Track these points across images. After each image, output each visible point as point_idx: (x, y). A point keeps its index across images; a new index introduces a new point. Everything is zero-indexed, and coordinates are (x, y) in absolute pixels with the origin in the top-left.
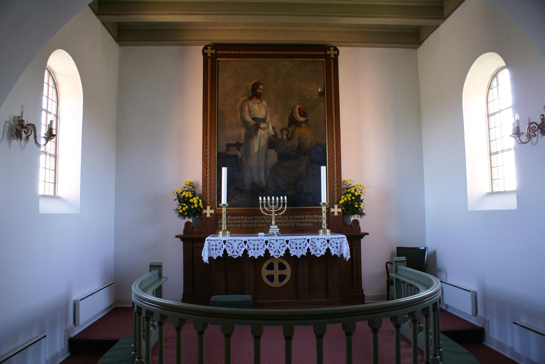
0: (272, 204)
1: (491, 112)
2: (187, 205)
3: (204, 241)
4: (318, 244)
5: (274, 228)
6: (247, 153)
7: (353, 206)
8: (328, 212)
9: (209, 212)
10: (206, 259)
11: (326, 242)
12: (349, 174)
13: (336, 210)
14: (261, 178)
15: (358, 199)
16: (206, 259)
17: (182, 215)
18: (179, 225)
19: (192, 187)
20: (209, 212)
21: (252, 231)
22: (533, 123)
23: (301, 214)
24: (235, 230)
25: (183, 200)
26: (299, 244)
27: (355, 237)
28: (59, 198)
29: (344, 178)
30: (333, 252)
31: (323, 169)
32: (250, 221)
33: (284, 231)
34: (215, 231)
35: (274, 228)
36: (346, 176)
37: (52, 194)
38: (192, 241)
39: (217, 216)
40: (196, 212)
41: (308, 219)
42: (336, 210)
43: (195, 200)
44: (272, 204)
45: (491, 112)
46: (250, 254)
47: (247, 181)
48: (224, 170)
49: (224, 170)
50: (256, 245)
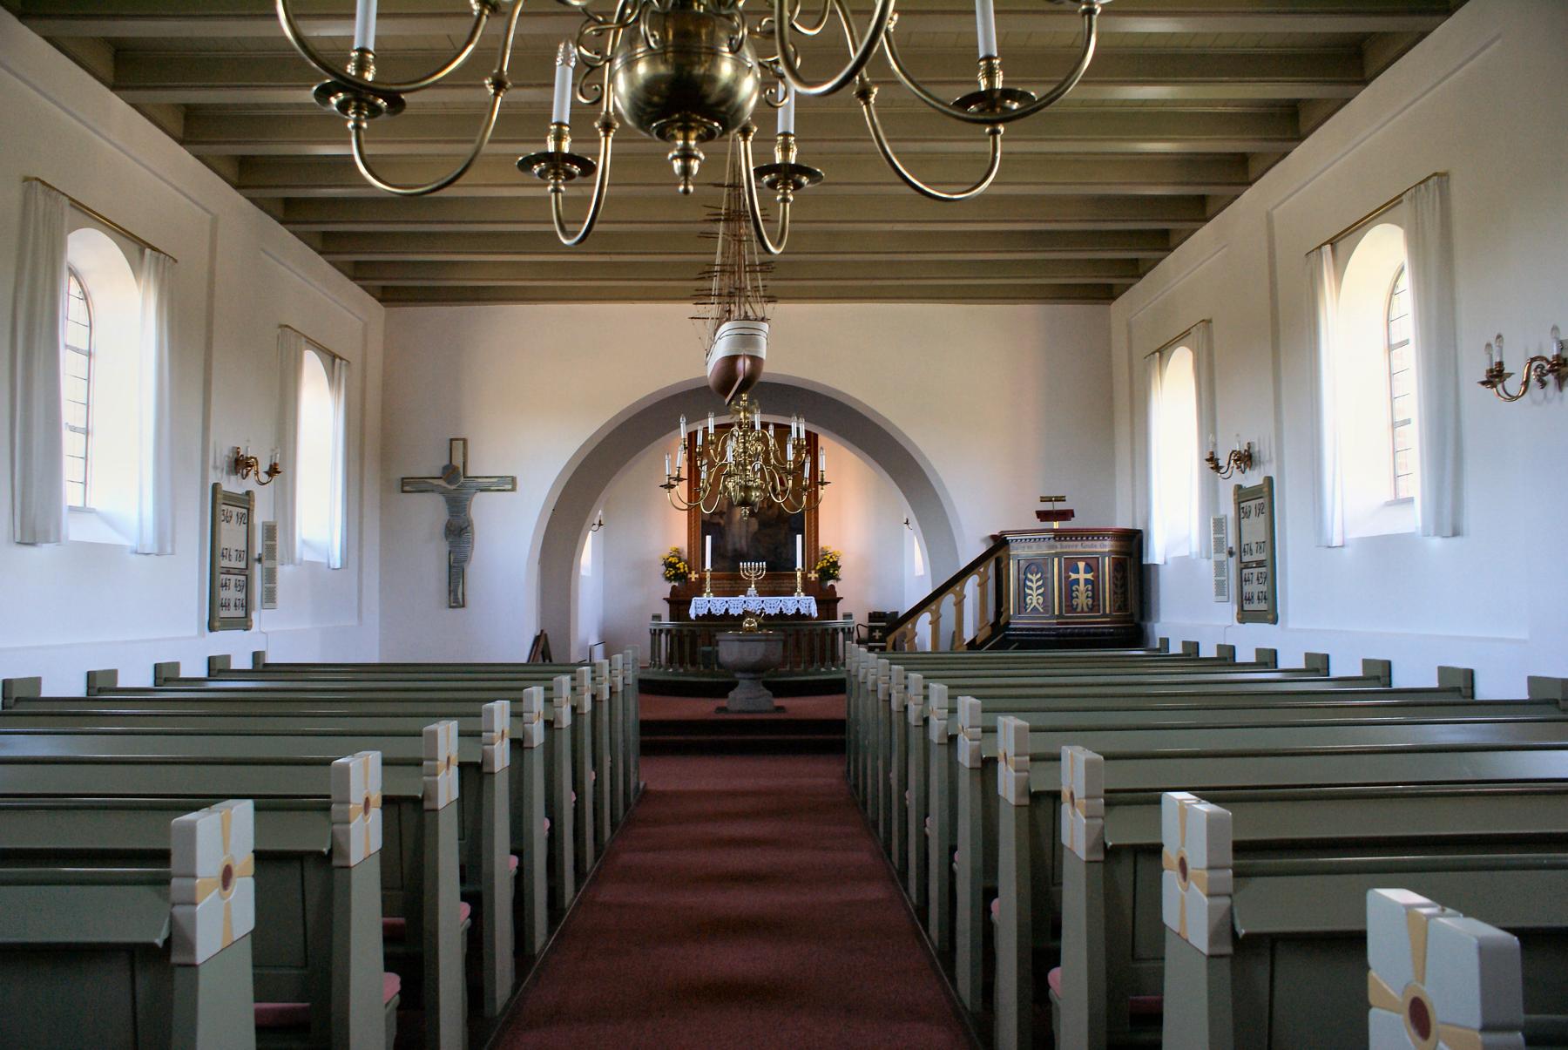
0: (752, 569)
1: (1394, 341)
2: (675, 572)
3: (689, 603)
4: (790, 604)
5: (752, 589)
6: (730, 521)
7: (830, 570)
8: (804, 577)
9: (694, 576)
10: (693, 616)
11: (804, 603)
12: (827, 540)
13: (813, 576)
14: (742, 544)
15: (835, 565)
16: (693, 616)
17: (669, 579)
18: (666, 588)
19: (677, 553)
20: (694, 576)
21: (734, 593)
22: (1533, 360)
23: (778, 579)
24: (718, 593)
25: (669, 565)
26: (773, 605)
27: (828, 603)
28: (92, 511)
29: (821, 544)
30: (802, 611)
31: (799, 537)
32: (734, 586)
33: (761, 593)
34: (700, 593)
35: (752, 589)
36: (823, 542)
37: (80, 504)
38: (678, 603)
39: (702, 580)
40: (680, 576)
41: (786, 583)
42: (813, 576)
43: (681, 565)
44: (752, 569)
45: (1394, 341)
46: (731, 612)
47: (730, 547)
48: (708, 538)
49: (708, 538)
50: (736, 605)
